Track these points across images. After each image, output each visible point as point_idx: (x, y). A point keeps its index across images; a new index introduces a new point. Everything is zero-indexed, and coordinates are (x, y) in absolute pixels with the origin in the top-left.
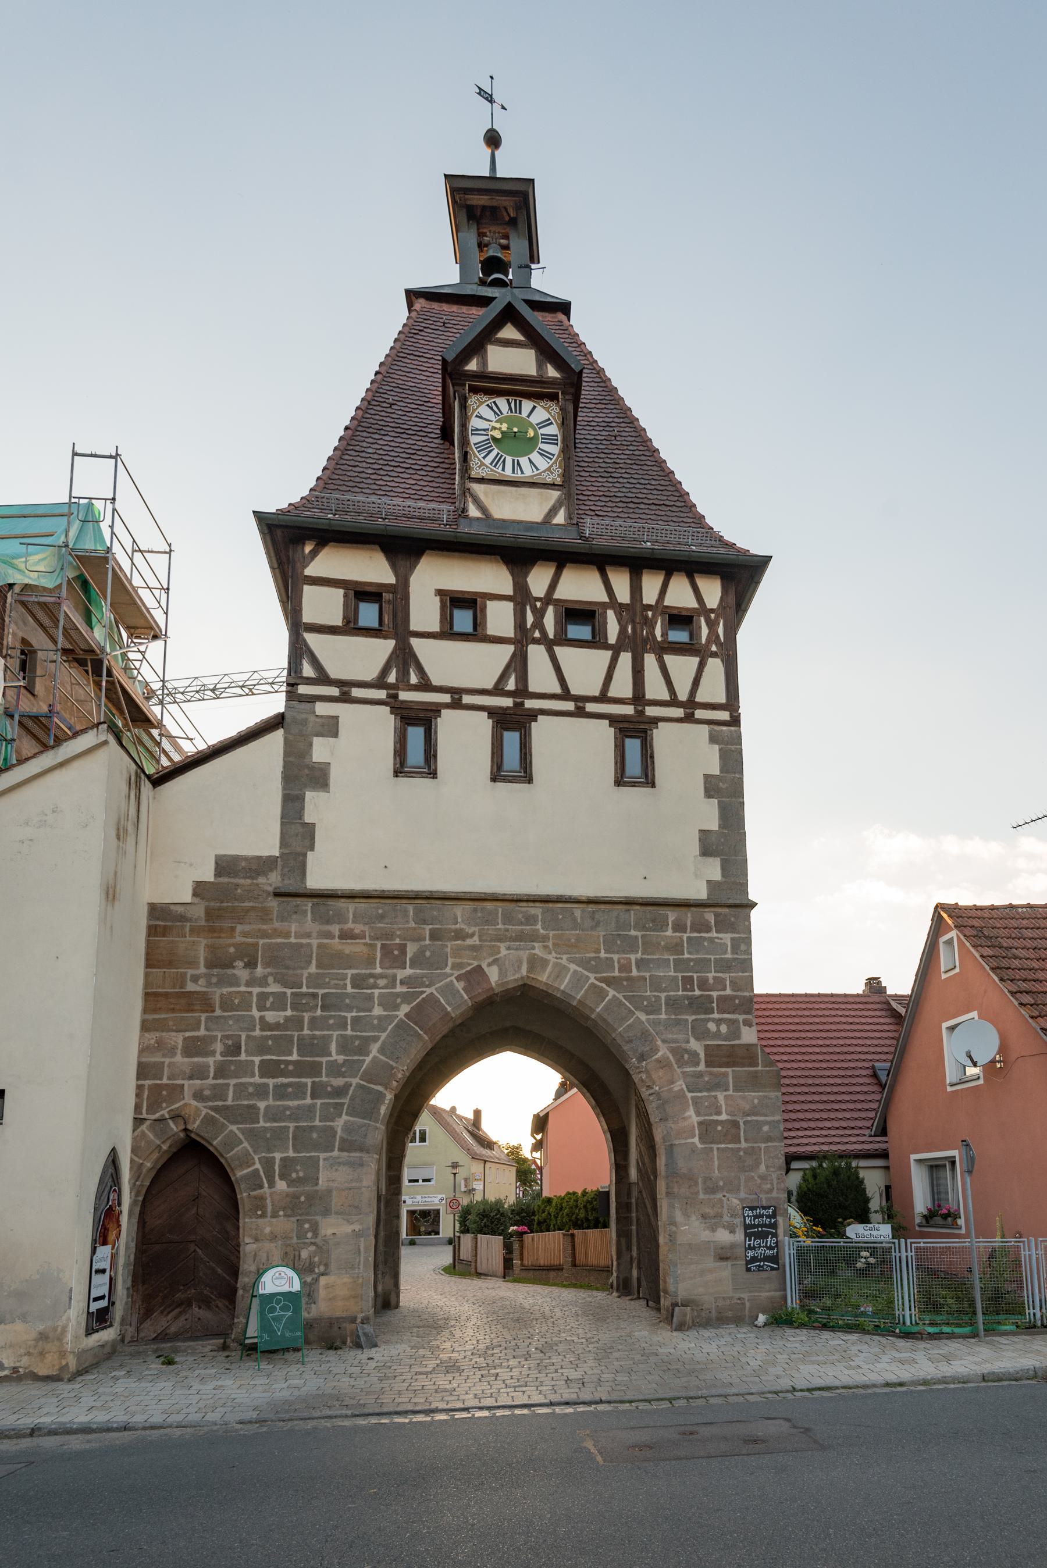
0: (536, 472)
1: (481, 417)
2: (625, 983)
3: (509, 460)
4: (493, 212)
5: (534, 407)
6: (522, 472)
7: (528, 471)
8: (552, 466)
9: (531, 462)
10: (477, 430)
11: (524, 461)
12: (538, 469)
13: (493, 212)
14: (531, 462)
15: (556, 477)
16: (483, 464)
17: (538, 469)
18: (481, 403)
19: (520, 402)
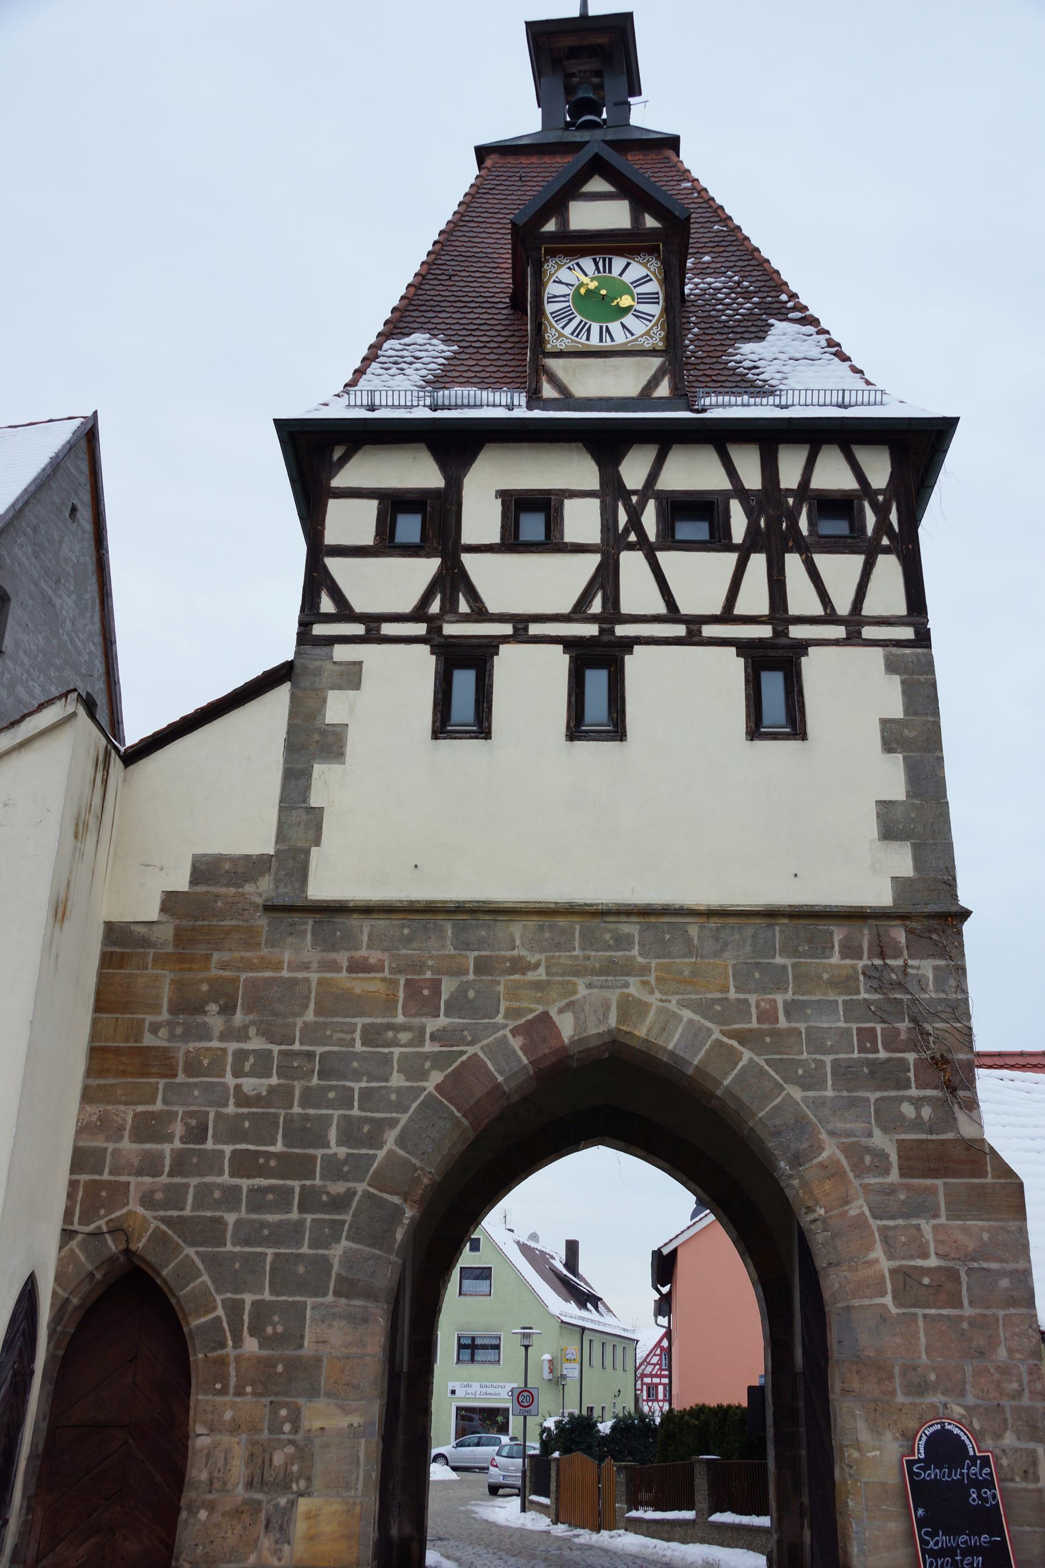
0: (631, 338)
3: (595, 328)
5: (628, 264)
7: (620, 338)
10: (555, 297)
11: (615, 327)
12: (633, 334)
15: (657, 340)
16: (561, 335)
18: (560, 267)
19: (610, 260)
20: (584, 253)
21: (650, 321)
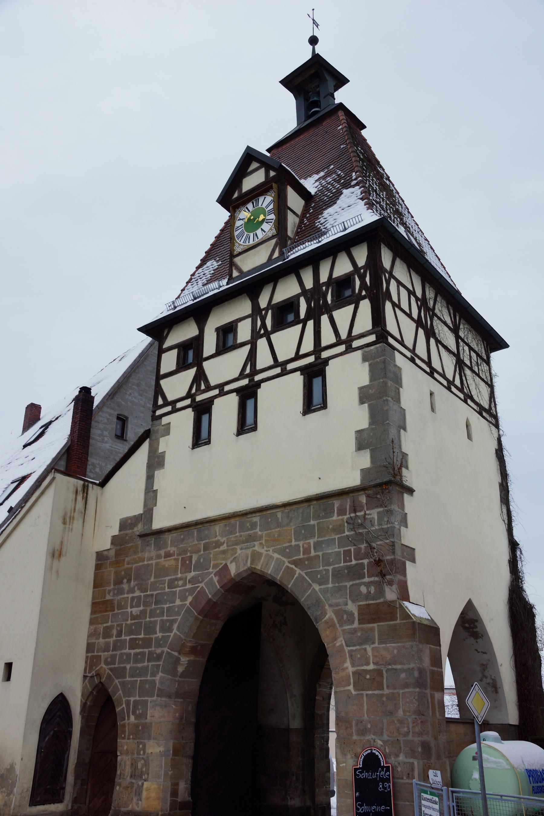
1: (240, 219)
2: (306, 563)
4: (313, 82)
6: (258, 238)
8: (241, 245)
9: (262, 230)
11: (259, 232)
13: (313, 82)
14: (262, 230)
15: (274, 232)
16: (240, 245)
17: (265, 232)
19: (247, 208)
20: (247, 202)
21: (271, 222)
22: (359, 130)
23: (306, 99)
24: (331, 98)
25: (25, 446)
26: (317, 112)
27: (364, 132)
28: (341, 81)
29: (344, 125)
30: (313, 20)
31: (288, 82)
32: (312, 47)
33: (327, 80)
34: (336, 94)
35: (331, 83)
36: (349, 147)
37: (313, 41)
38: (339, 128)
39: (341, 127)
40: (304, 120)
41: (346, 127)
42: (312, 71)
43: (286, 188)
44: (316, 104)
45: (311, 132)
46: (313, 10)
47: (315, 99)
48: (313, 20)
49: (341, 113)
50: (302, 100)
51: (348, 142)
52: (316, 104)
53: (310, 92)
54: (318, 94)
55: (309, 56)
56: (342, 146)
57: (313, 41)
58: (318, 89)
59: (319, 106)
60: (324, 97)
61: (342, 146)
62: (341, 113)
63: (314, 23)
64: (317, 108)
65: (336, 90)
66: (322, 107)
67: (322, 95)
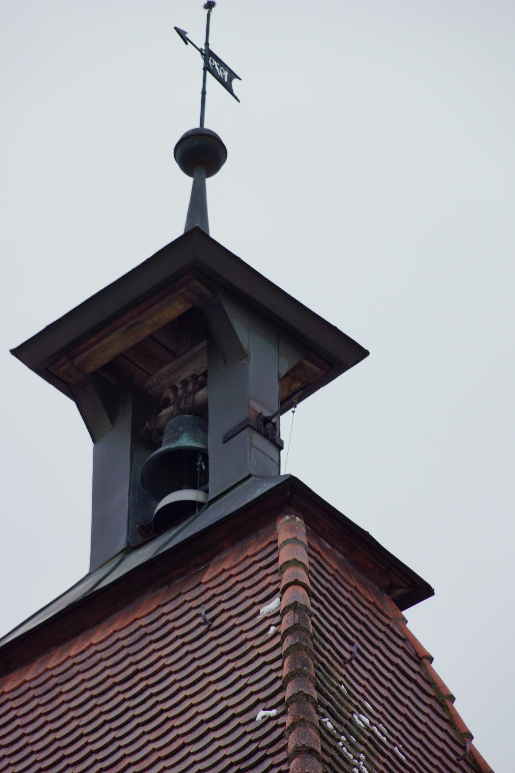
22: (390, 607)
23: (144, 439)
24: (258, 440)
25: (239, 101)
26: (186, 509)
27: (418, 619)
28: (321, 353)
29: (289, 596)
30: (208, 54)
31: (50, 354)
32: (189, 181)
33: (244, 355)
34: (287, 422)
35: (264, 362)
36: (288, 720)
37: (200, 153)
38: (267, 609)
39: (273, 605)
40: (122, 544)
41: (294, 607)
42: (173, 309)
43: (402, 614)
44: (189, 467)
45: (143, 615)
46: (210, 6)
47: (185, 441)
48: (208, 54)
49: (289, 533)
50: (122, 439)
51: (288, 693)
52: (189, 467)
53: (166, 403)
54: (200, 415)
55: (176, 229)
56: (261, 714)
57: (200, 153)
58: (201, 393)
59: (199, 481)
60: (227, 439)
61: (261, 714)
62: (289, 533)
63: (207, 68)
64: (193, 486)
65: (288, 403)
66: (215, 485)
67: (218, 424)
